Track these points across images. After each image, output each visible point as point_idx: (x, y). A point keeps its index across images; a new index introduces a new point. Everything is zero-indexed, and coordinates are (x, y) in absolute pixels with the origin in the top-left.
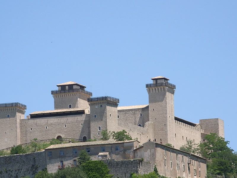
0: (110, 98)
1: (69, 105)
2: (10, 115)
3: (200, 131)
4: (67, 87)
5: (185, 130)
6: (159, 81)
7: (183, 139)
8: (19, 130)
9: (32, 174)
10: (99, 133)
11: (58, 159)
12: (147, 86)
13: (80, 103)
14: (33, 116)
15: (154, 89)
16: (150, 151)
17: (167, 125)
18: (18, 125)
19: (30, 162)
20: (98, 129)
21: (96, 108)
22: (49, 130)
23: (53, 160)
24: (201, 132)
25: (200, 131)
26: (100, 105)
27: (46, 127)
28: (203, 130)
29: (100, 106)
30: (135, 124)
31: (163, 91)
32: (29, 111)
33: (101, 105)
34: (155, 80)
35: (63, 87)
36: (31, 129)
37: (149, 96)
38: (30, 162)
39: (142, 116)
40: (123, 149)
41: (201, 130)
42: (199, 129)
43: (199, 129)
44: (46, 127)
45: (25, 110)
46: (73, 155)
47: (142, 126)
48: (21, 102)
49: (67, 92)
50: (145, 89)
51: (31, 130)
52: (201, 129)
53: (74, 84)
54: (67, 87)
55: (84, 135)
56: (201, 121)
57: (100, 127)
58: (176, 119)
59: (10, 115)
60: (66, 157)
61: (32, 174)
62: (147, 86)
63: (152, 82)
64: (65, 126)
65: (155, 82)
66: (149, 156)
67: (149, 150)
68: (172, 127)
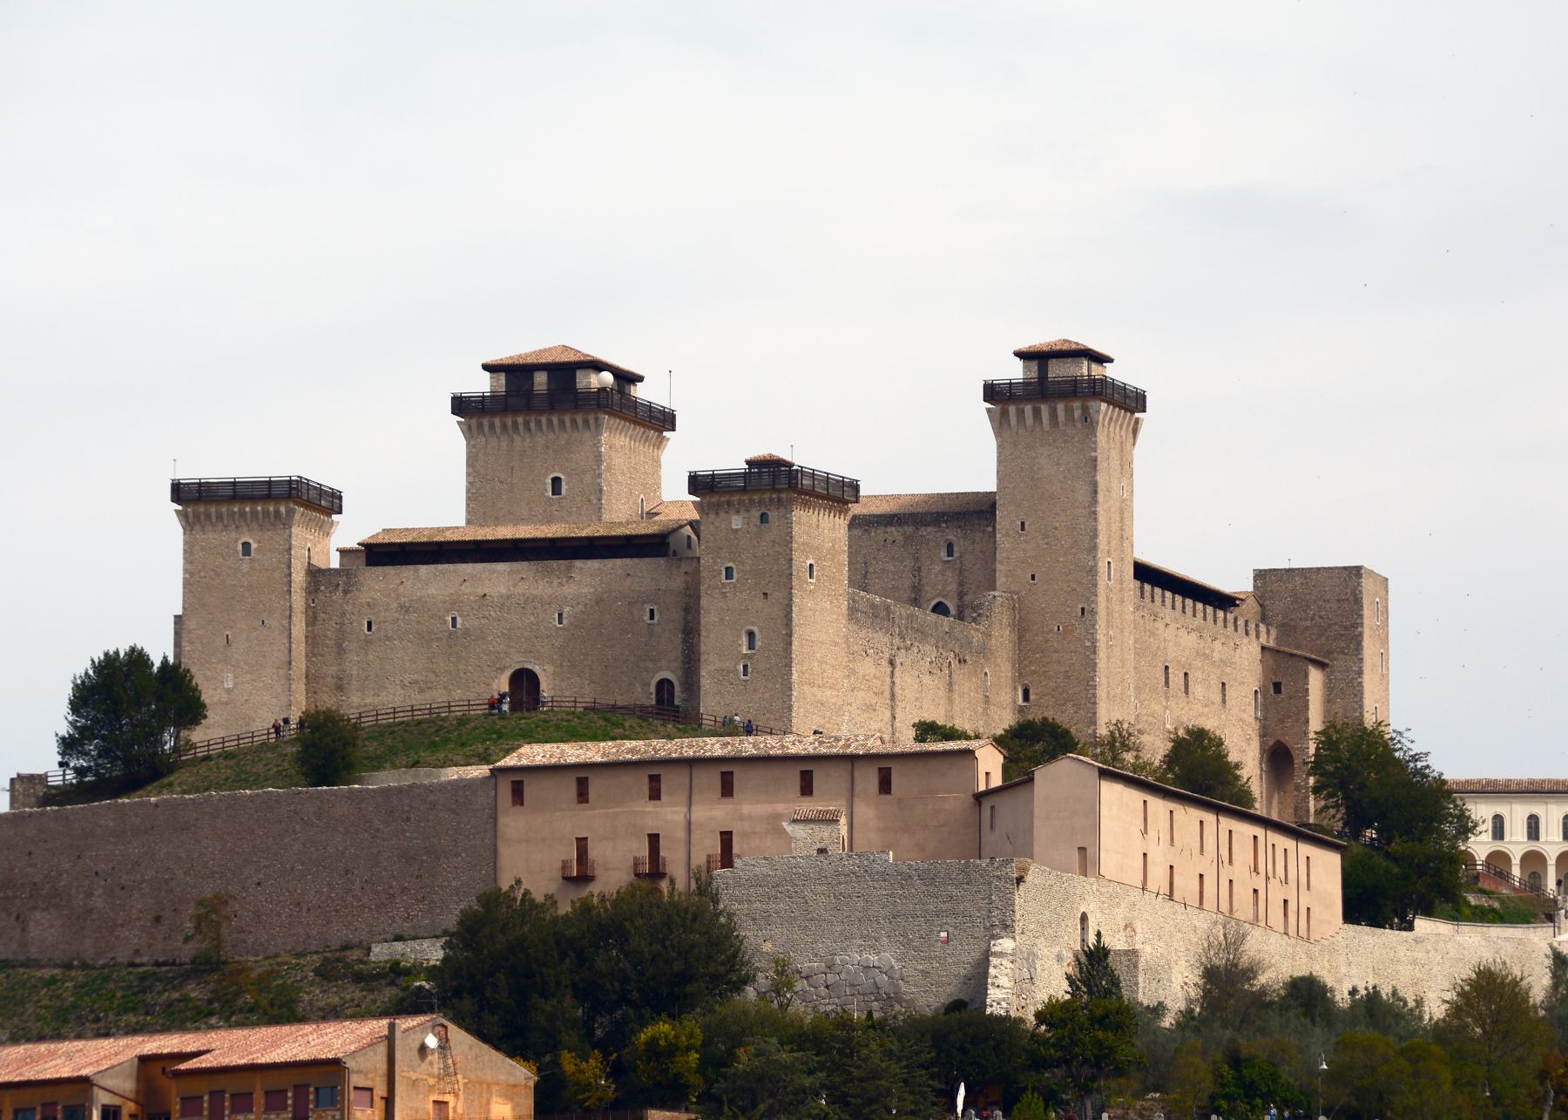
0: (813, 475)
3: (1258, 637)
4: (541, 379)
5: (1180, 631)
6: (1057, 370)
7: (1167, 683)
8: (299, 628)
10: (745, 667)
12: (992, 392)
13: (609, 468)
14: (383, 554)
15: (1028, 409)
17: (1093, 612)
18: (298, 600)
20: (744, 639)
22: (466, 633)
24: (1263, 640)
25: (1258, 637)
26: (756, 514)
27: (454, 619)
28: (1273, 632)
30: (915, 602)
32: (351, 530)
33: (763, 510)
35: (515, 374)
36: (369, 624)
37: (1000, 447)
39: (956, 554)
41: (1263, 628)
42: (1252, 626)
43: (1252, 626)
44: (454, 619)
47: (953, 611)
48: (321, 474)
49: (543, 401)
50: (980, 408)
51: (369, 629)
52: (1264, 619)
54: (541, 379)
55: (661, 669)
56: (1261, 576)
57: (751, 634)
58: (1145, 573)
59: (254, 546)
62: (992, 392)
63: (1015, 371)
64: (560, 615)
65: (1034, 373)
68: (1125, 634)
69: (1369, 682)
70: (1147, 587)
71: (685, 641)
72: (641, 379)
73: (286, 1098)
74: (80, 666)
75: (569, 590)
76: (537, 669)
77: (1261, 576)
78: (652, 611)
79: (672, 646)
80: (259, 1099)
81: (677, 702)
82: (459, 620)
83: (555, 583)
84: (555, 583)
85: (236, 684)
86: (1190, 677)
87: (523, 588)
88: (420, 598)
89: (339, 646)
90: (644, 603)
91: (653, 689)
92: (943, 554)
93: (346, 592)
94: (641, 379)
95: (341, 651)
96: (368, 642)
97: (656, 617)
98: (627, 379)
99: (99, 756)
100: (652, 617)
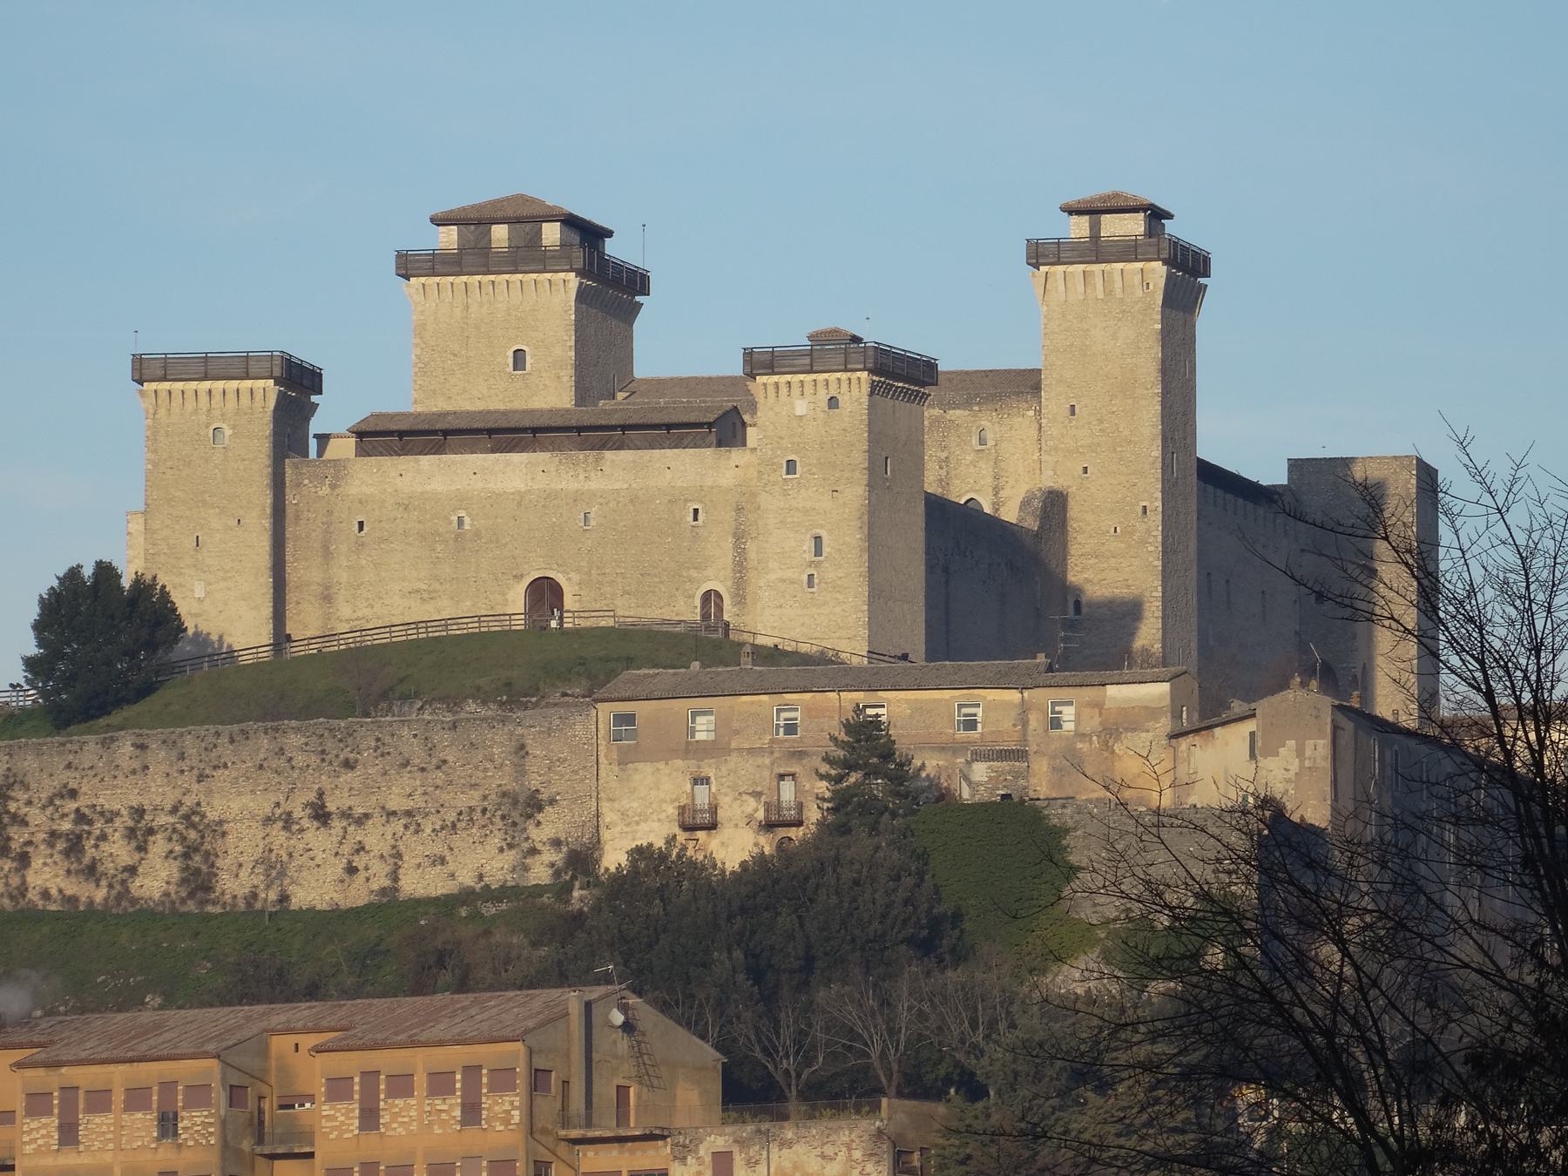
1: (510, 354)
2: (234, 427)
9: (501, 850)
11: (679, 763)
14: (384, 437)
16: (1300, 753)
19: (486, 770)
21: (799, 412)
23: (640, 766)
29: (824, 405)
31: (1139, 293)
34: (1087, 218)
38: (486, 770)
39: (991, 443)
40: (1097, 720)
45: (314, 398)
46: (772, 741)
53: (1167, 439)
56: (1296, 466)
58: (1211, 475)
59: (228, 432)
60: (727, 751)
61: (501, 850)
66: (1288, 781)
67: (1291, 743)
69: (383, 638)
70: (1210, 488)
71: (736, 546)
72: (610, 234)
73: (454, 1081)
74: (47, 580)
75: (596, 483)
76: (561, 579)
77: (1296, 466)
78: (696, 511)
79: (721, 552)
80: (421, 1081)
81: (726, 617)
82: (467, 520)
83: (581, 477)
84: (581, 477)
85: (207, 593)
86: (158, 344)
87: (542, 482)
88: (422, 493)
89: (326, 548)
90: (686, 501)
91: (698, 602)
92: (975, 441)
93: (333, 487)
94: (610, 234)
95: (327, 554)
96: (361, 545)
97: (701, 516)
98: (1156, 216)
99: (1371, 948)
100: (696, 519)
